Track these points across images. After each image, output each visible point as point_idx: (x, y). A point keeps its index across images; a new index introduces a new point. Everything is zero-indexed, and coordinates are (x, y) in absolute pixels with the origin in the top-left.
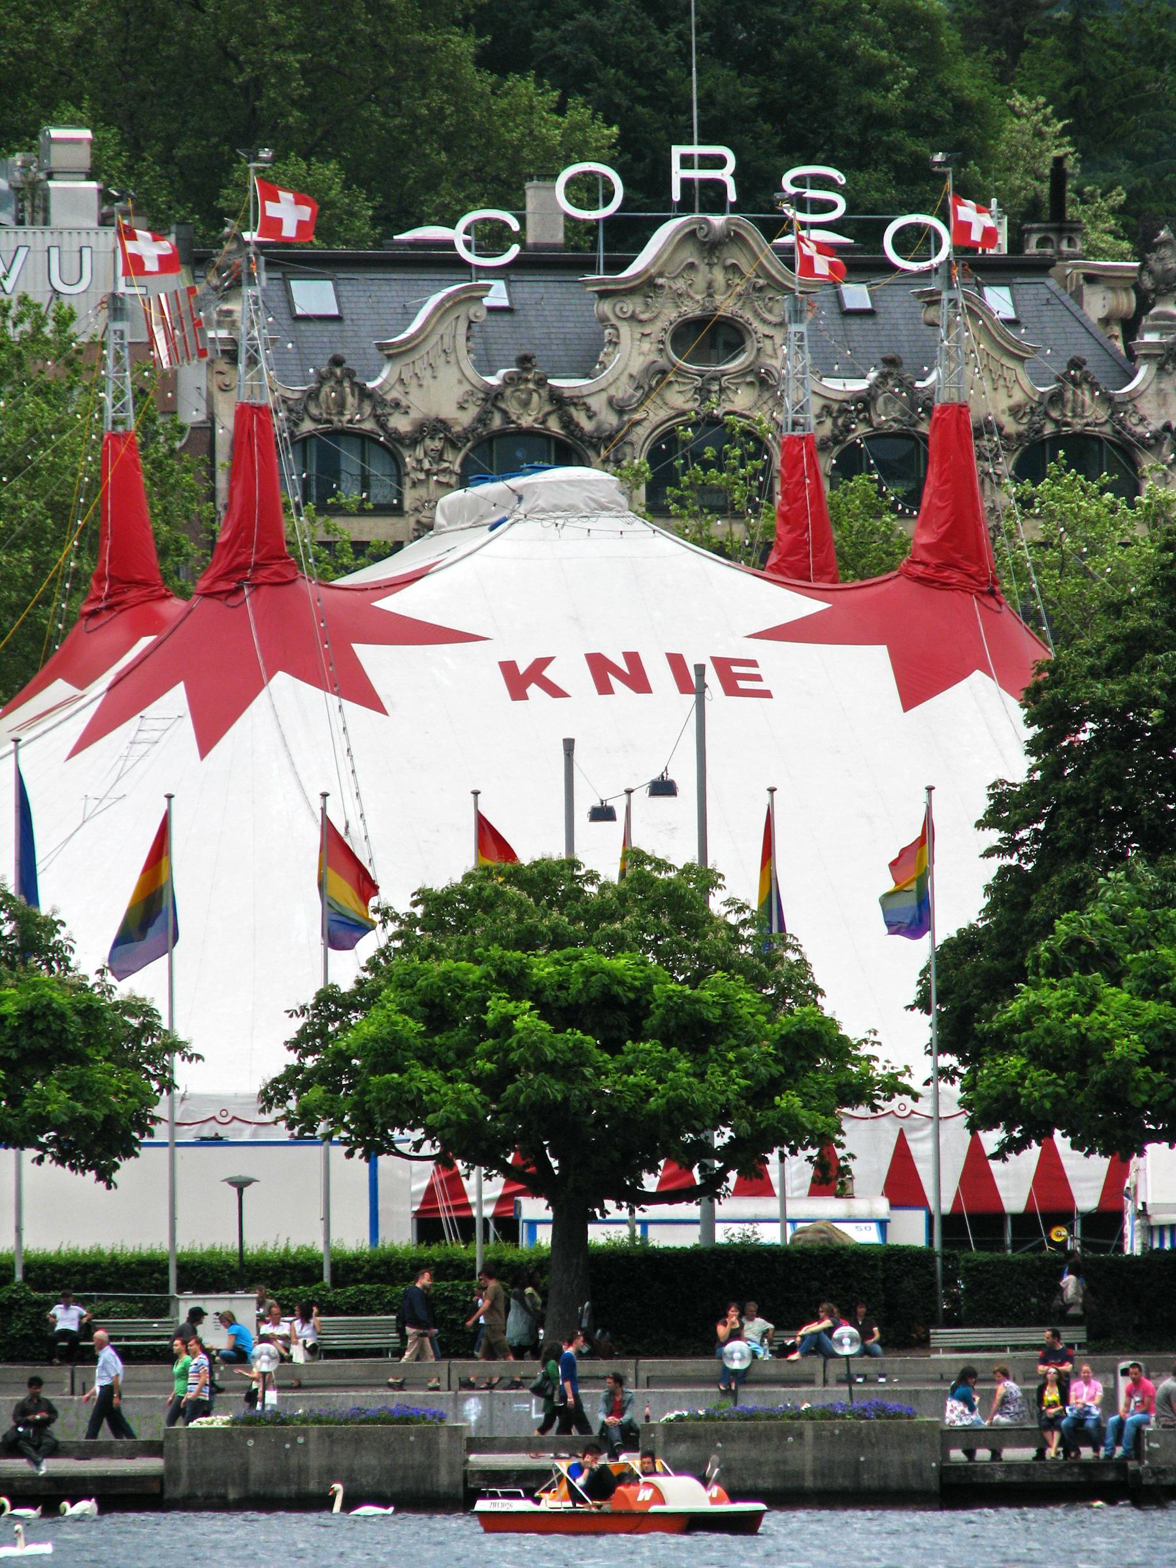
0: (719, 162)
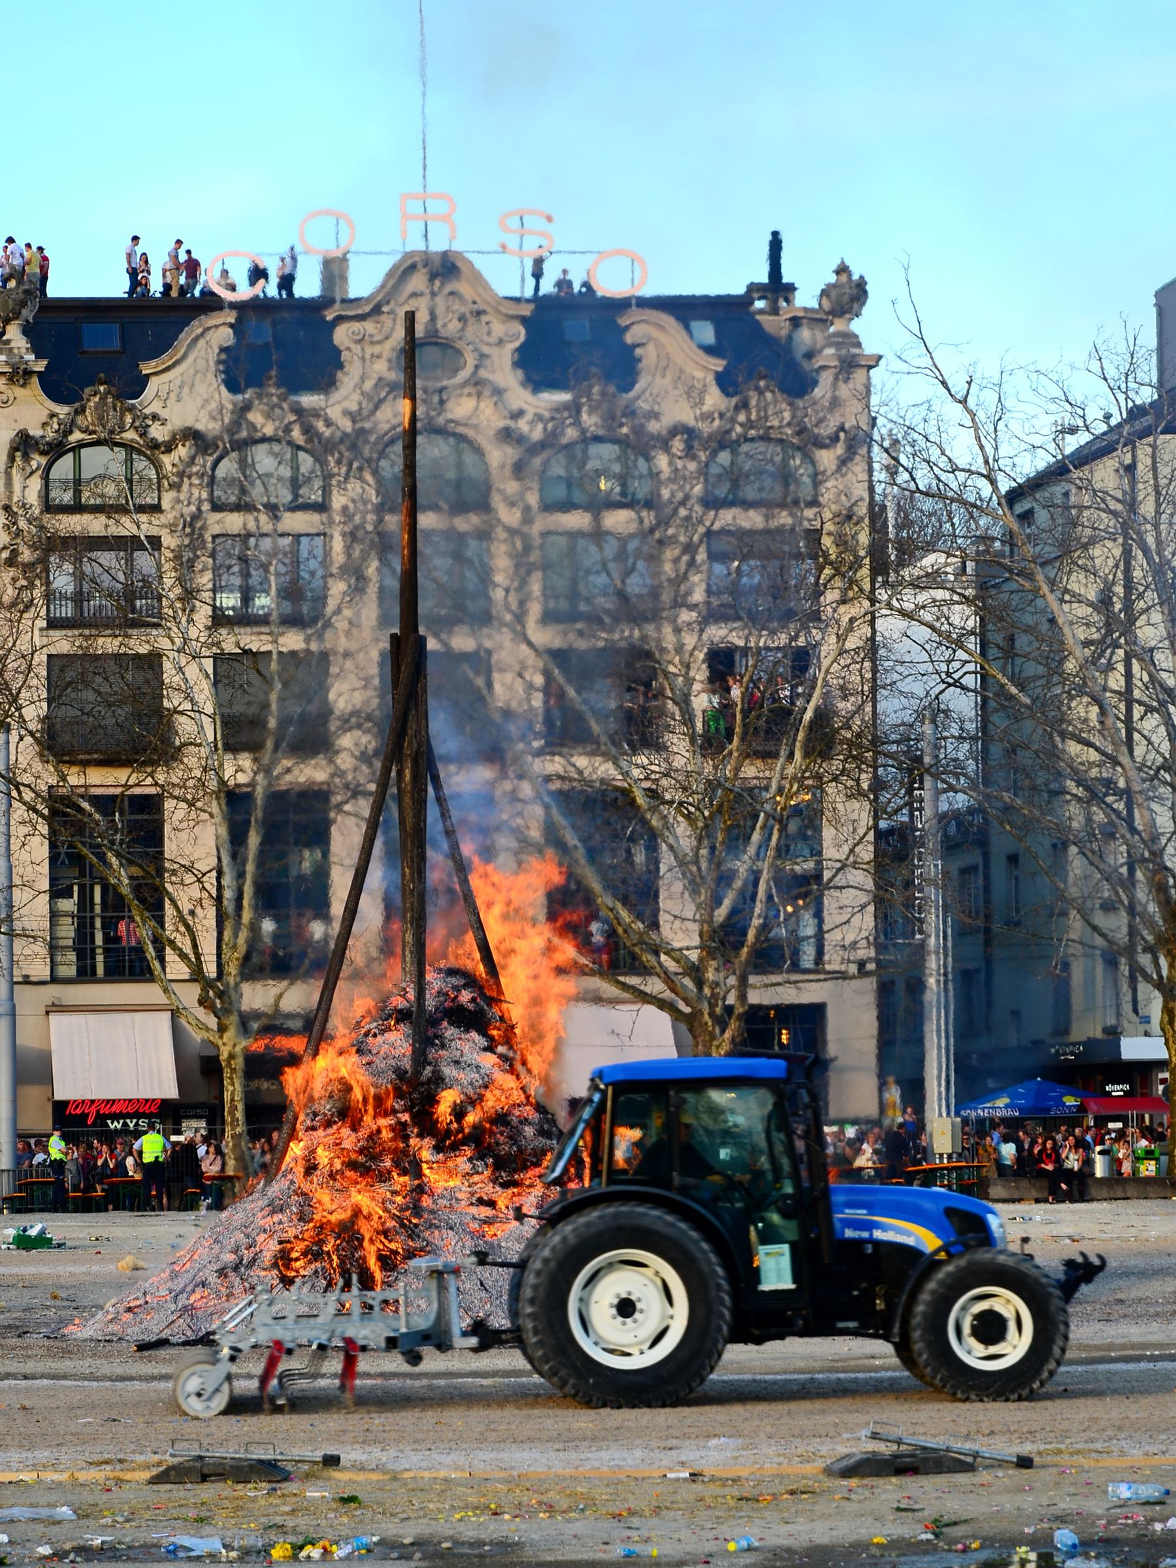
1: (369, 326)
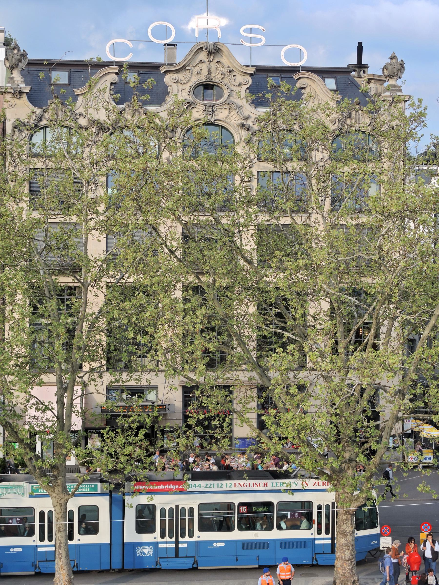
1: (180, 76)
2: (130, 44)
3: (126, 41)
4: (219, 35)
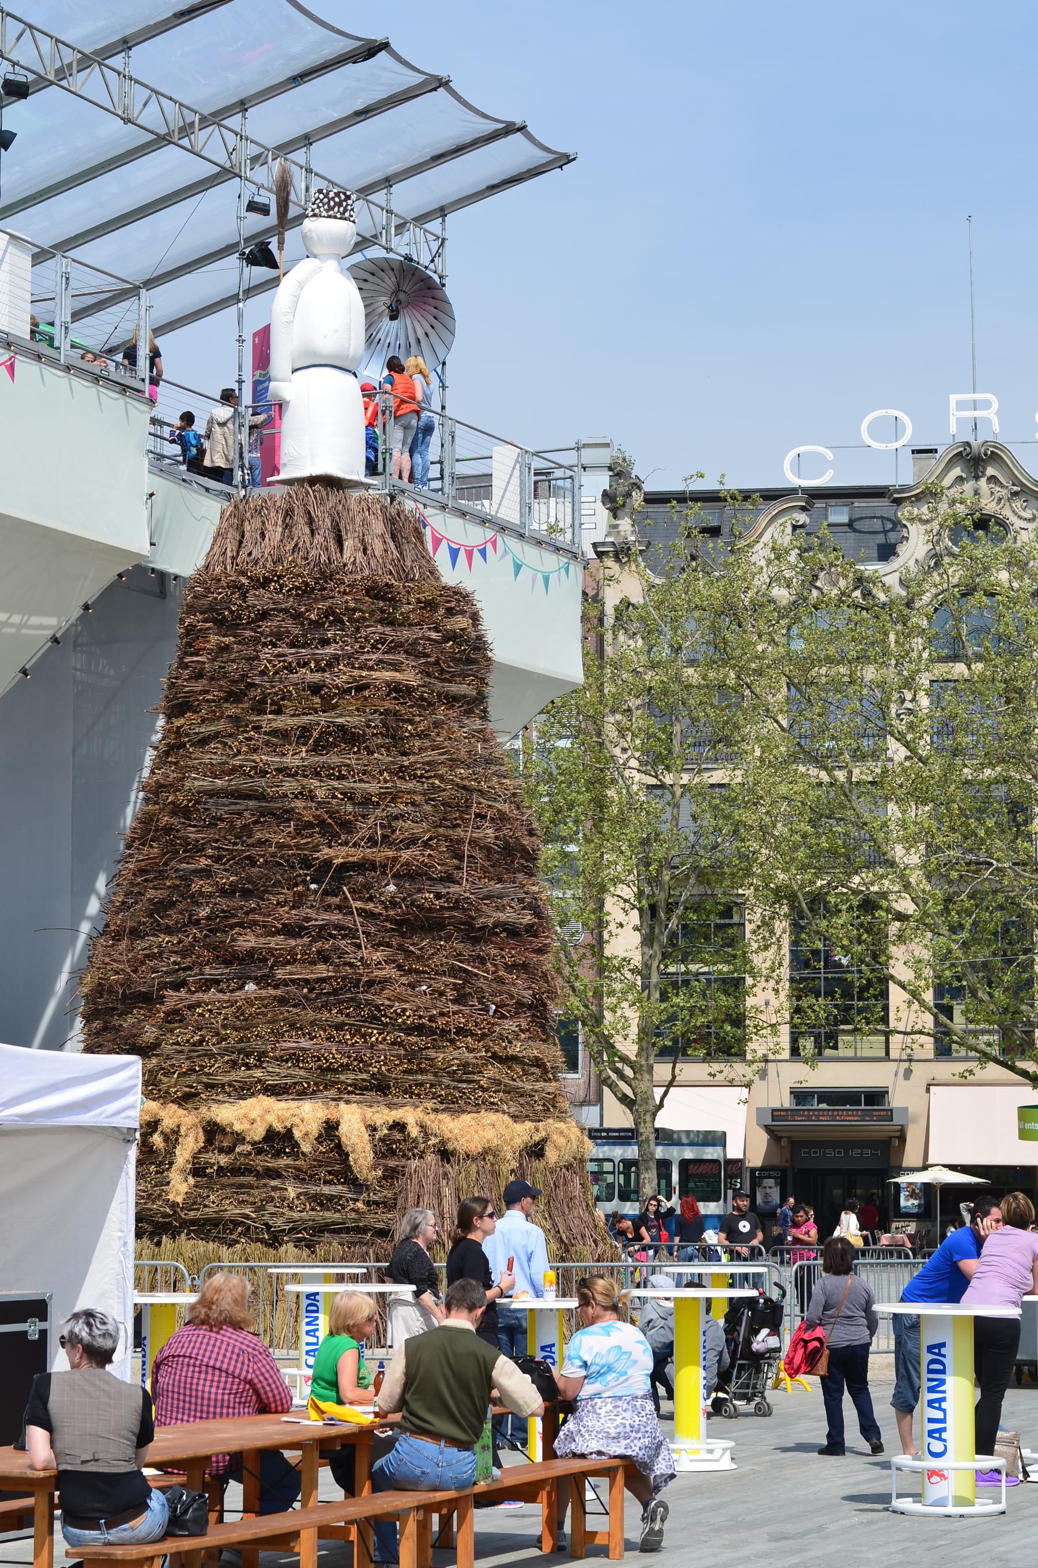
0: (987, 405)
1: (924, 510)
2: (829, 455)
3: (821, 449)
4: (996, 428)
